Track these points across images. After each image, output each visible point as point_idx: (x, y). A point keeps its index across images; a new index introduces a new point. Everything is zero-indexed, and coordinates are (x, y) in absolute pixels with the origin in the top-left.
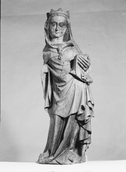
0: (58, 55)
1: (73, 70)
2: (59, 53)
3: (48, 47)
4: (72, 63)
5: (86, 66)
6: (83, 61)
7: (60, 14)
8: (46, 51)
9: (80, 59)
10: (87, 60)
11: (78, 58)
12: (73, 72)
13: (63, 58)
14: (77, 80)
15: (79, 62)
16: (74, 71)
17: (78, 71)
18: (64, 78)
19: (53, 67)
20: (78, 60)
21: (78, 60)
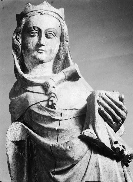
0: (46, 98)
1: (88, 128)
2: (48, 93)
3: (22, 85)
4: (84, 117)
5: (119, 118)
6: (110, 105)
7: (45, 12)
8: (16, 96)
9: (103, 99)
10: (121, 103)
11: (97, 98)
12: (89, 132)
13: (60, 105)
14: (103, 157)
15: (103, 109)
16: (91, 130)
17: (103, 132)
18: (67, 150)
19: (38, 84)
20: (100, 103)
21: (100, 103)
